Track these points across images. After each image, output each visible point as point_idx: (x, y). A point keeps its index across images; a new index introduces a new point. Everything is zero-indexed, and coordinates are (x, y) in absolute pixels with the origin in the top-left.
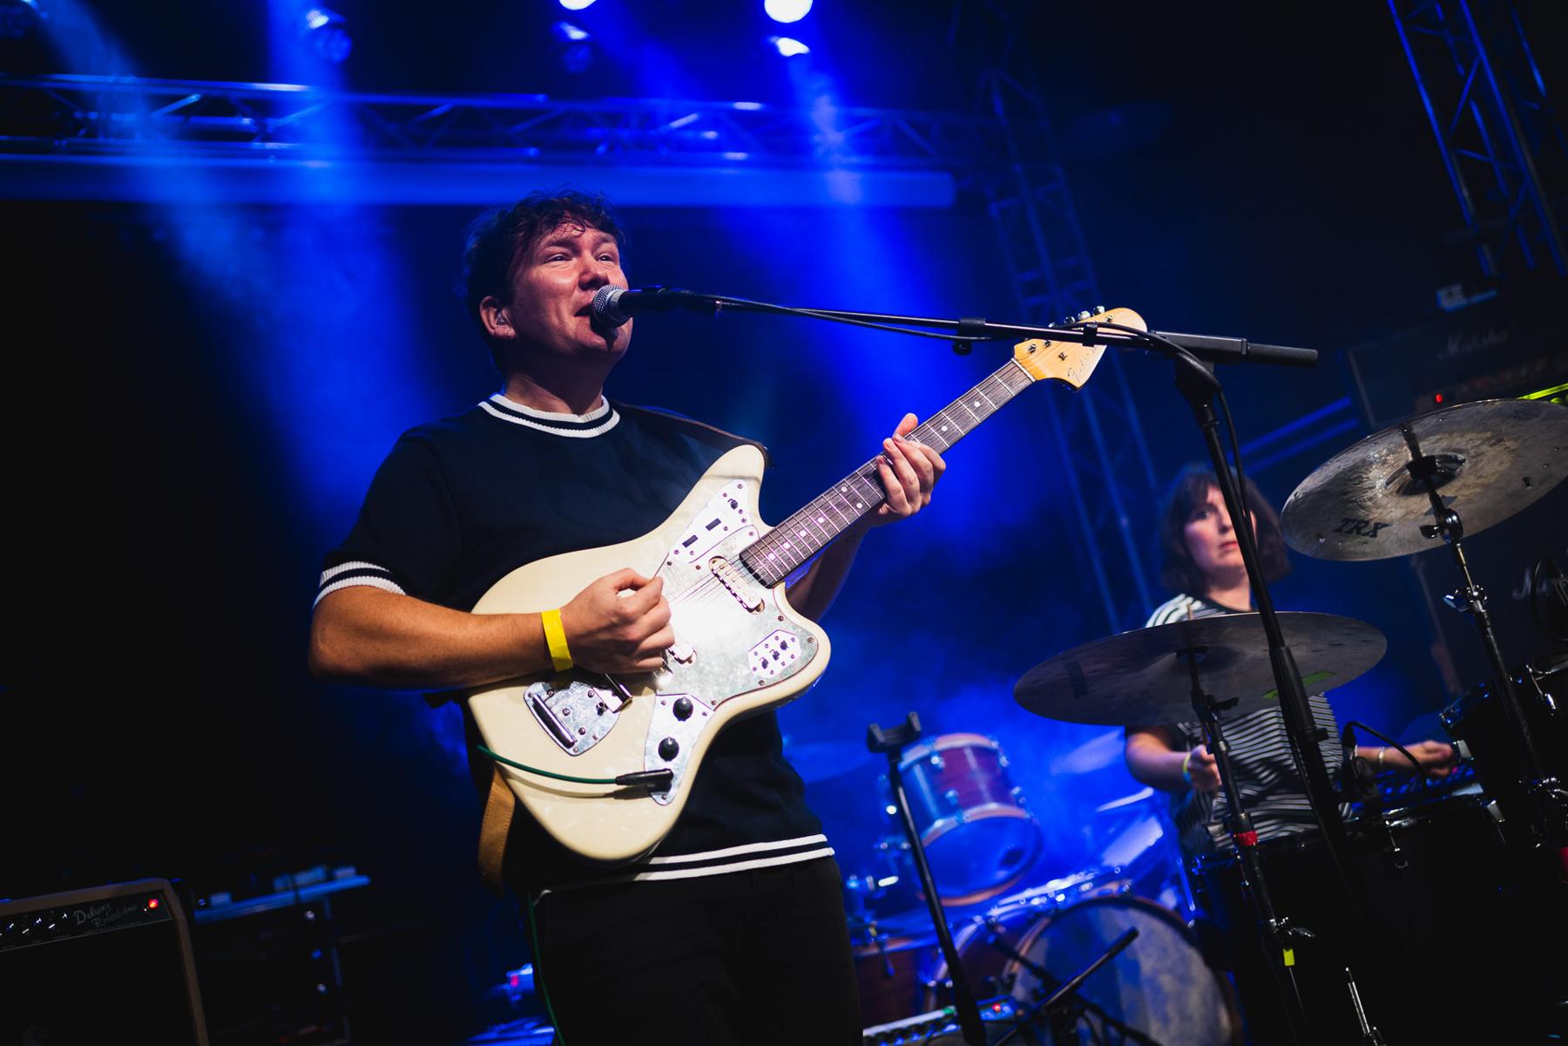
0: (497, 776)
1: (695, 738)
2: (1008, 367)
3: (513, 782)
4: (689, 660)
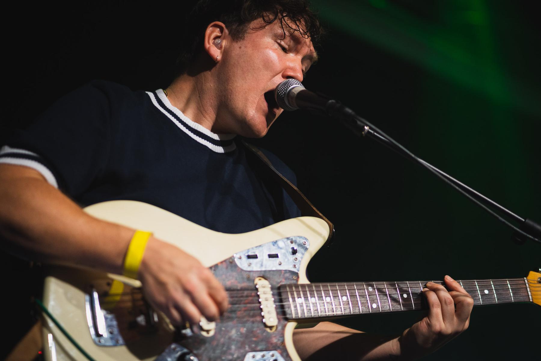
4: (271, 328)
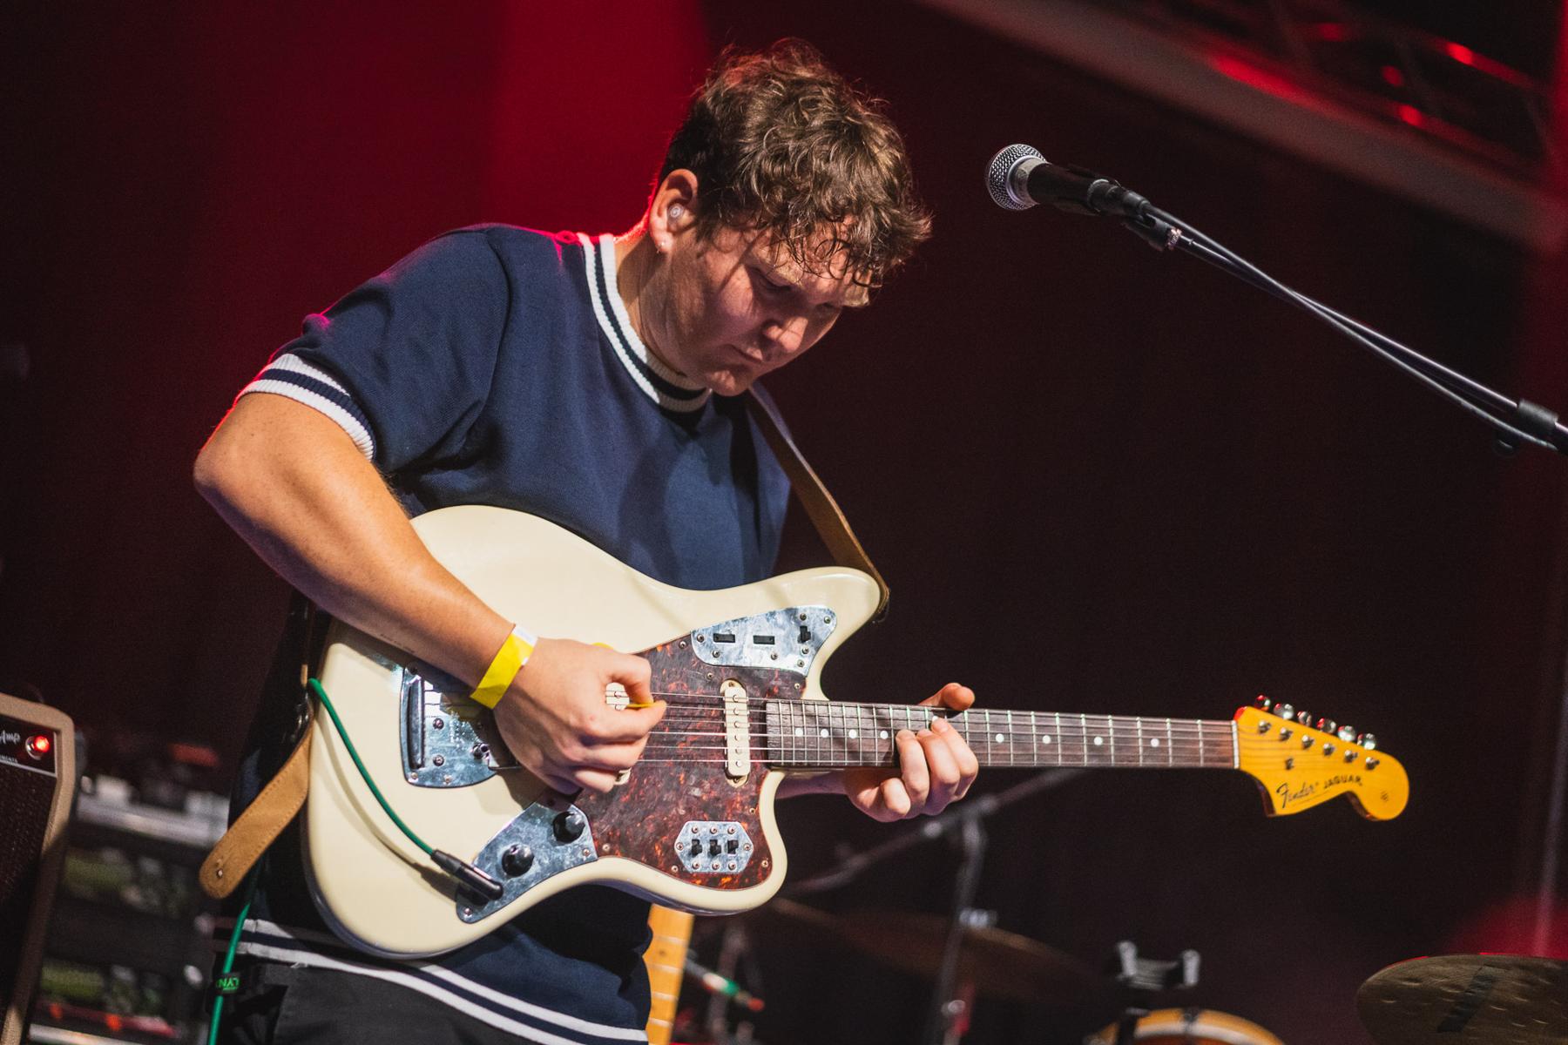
4: (737, 778)
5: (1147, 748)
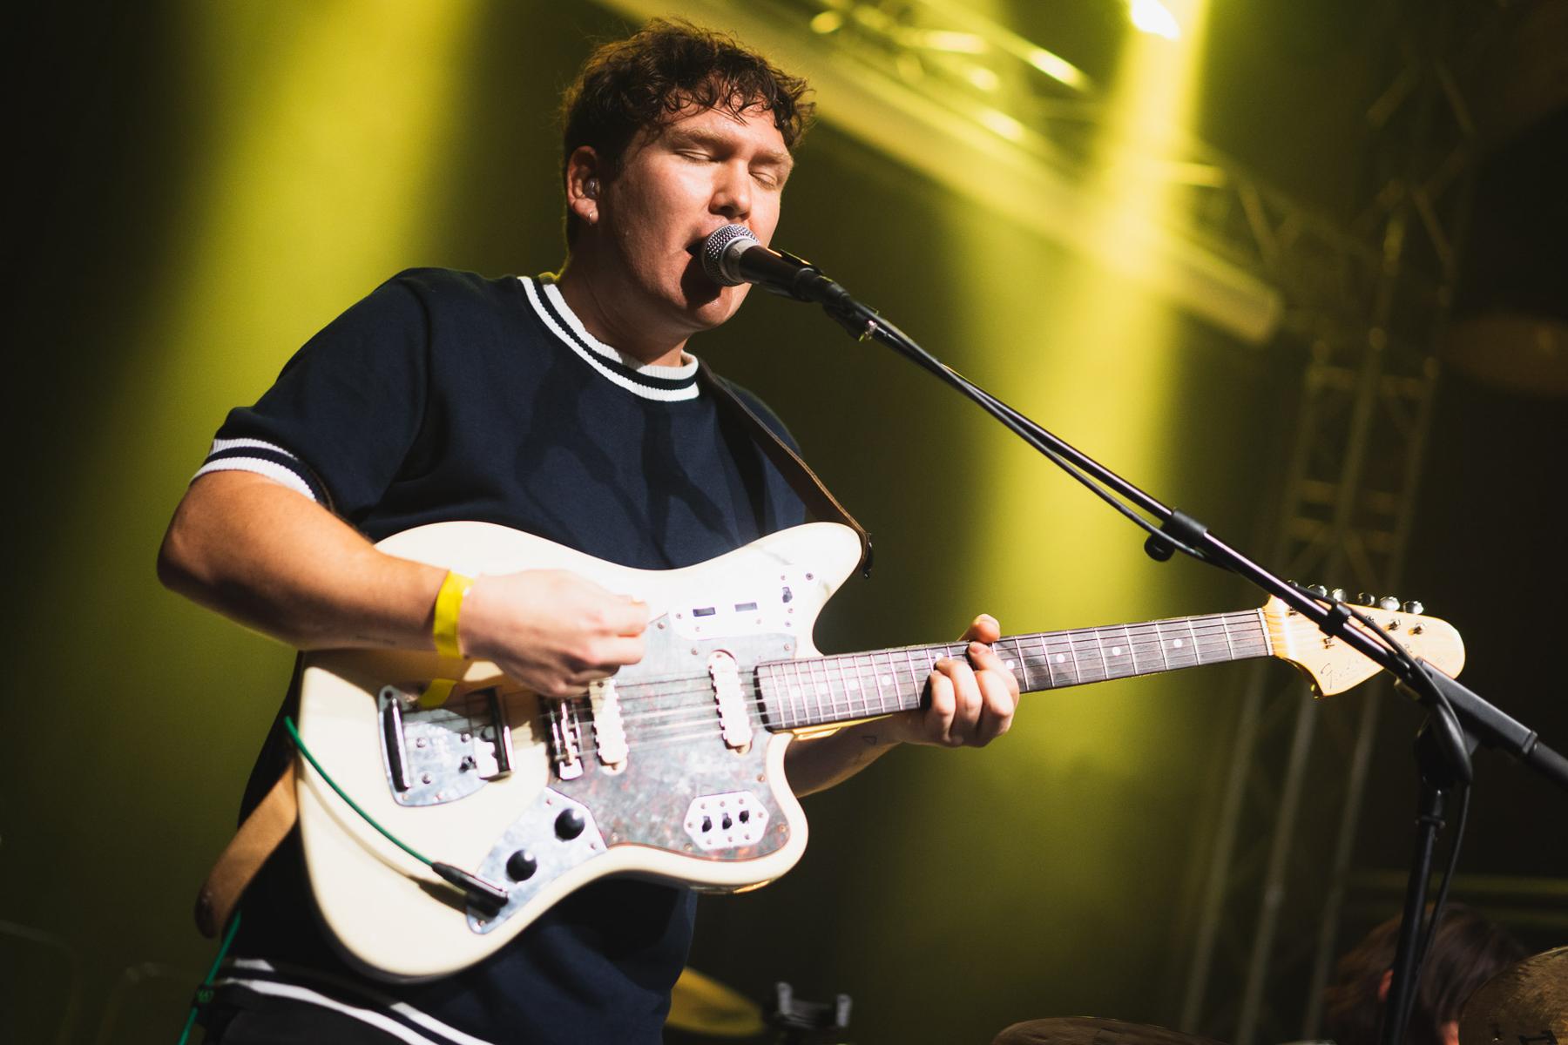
0: (288, 776)
1: (566, 870)
2: (1247, 616)
3: (302, 786)
5: (1172, 650)
